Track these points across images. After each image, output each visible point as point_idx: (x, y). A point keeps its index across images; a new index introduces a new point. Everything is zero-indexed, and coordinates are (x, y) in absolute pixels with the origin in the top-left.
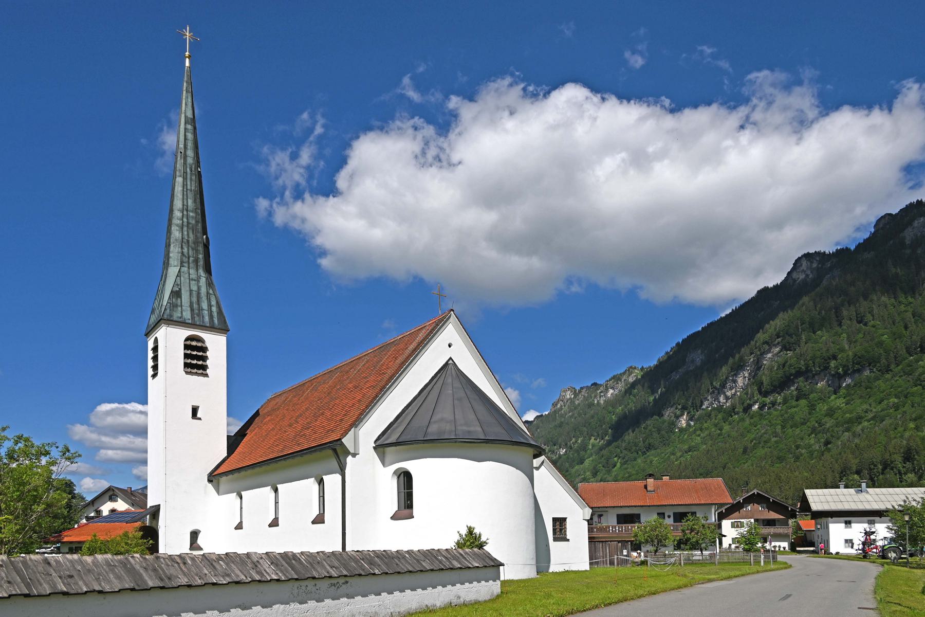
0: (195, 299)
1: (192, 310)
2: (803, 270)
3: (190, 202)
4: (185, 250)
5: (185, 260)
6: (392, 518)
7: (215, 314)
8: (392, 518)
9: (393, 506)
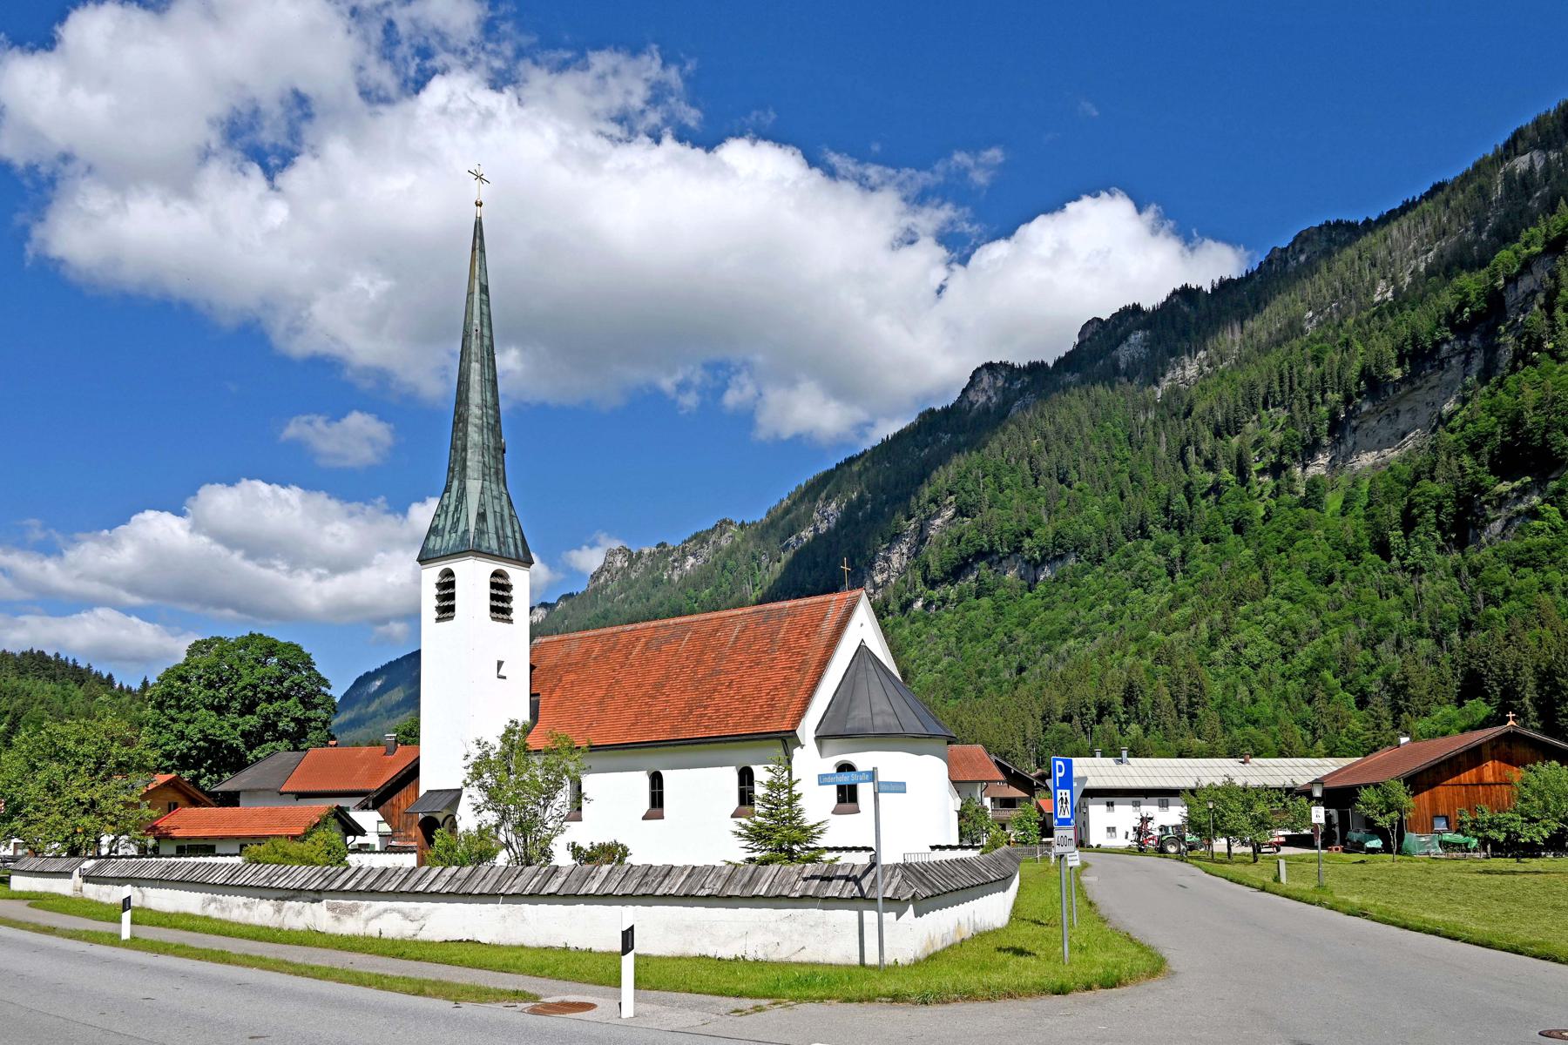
0: (499, 524)
1: (498, 538)
2: (984, 389)
4: (486, 459)
5: (487, 471)
6: (644, 818)
8: (644, 818)
9: (645, 804)
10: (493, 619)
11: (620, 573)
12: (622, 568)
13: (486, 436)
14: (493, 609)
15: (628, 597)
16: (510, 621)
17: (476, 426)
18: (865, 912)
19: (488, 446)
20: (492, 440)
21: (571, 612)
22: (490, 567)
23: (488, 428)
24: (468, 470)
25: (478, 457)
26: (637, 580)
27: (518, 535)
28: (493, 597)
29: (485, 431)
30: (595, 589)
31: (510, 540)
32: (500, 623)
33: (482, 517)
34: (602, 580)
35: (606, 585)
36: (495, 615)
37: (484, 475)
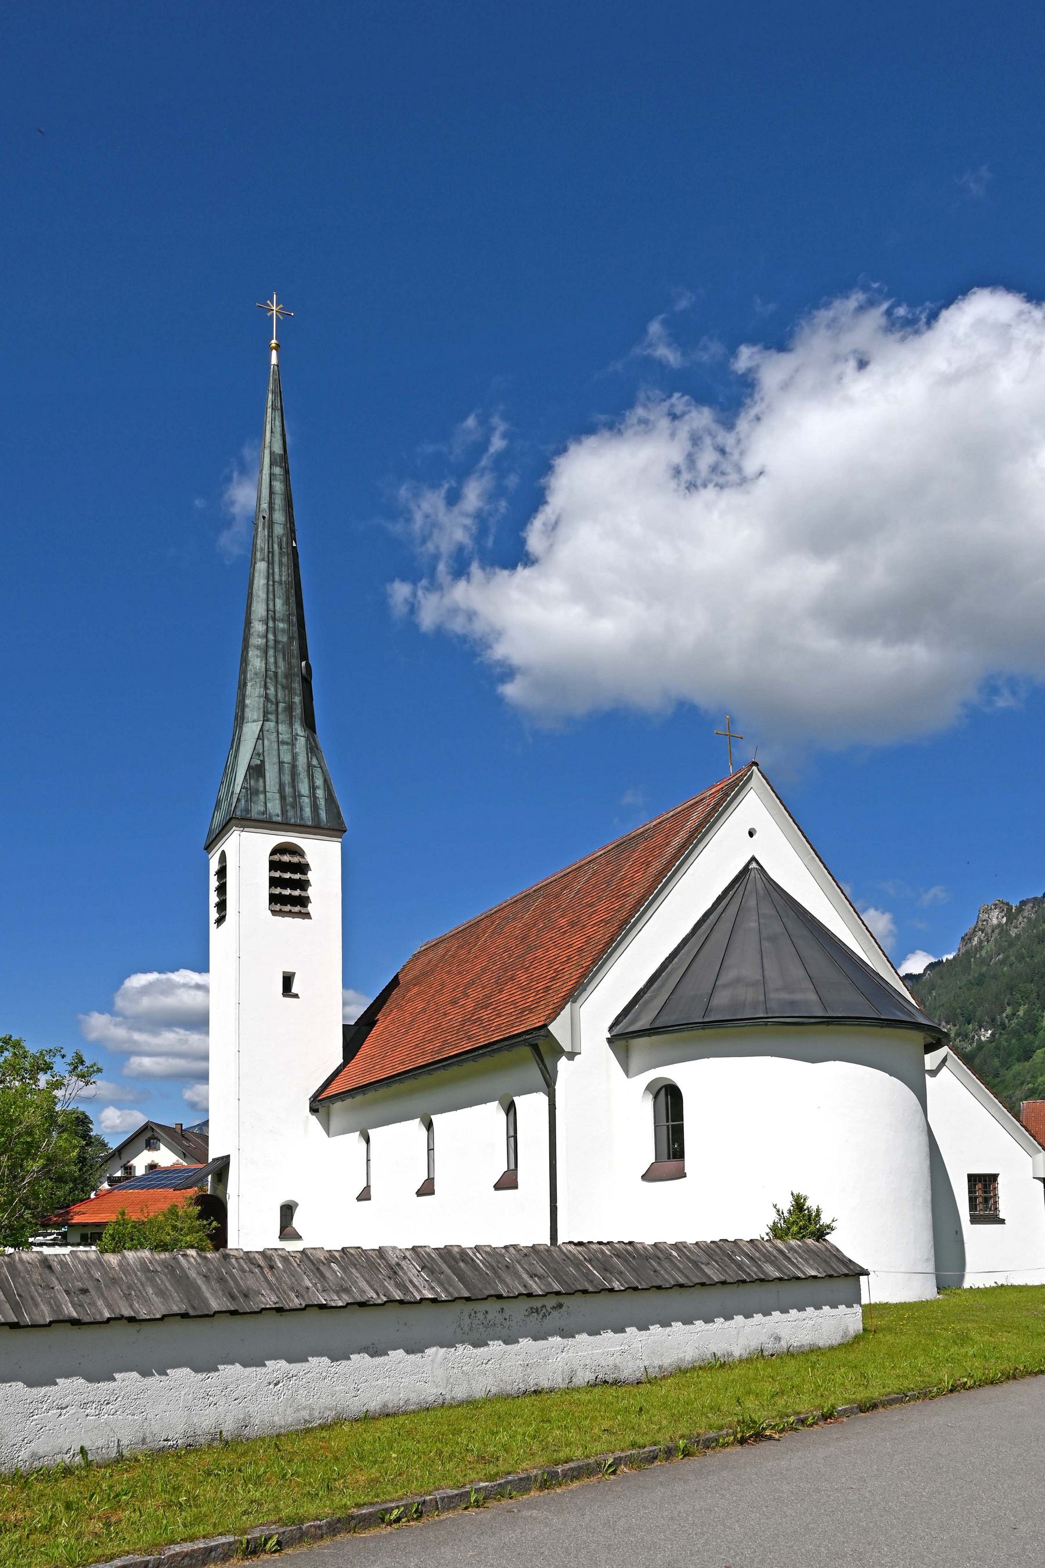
0: (287, 778)
1: (283, 798)
3: (279, 603)
5: (271, 708)
7: (322, 803)
9: (646, 1155)
10: (274, 913)
11: (997, 931)
12: (1000, 925)
13: (272, 660)
14: (273, 899)
15: (1006, 958)
16: (307, 916)
17: (258, 648)
18: (543, 1238)
19: (276, 674)
20: (281, 663)
21: (939, 981)
22: (267, 841)
23: (275, 648)
24: (247, 710)
25: (259, 691)
26: (1018, 936)
27: (320, 793)
28: (273, 882)
29: (271, 652)
30: (967, 952)
31: (306, 801)
32: (288, 920)
33: (256, 771)
34: (975, 941)
35: (980, 947)
36: (278, 907)
37: (266, 713)
